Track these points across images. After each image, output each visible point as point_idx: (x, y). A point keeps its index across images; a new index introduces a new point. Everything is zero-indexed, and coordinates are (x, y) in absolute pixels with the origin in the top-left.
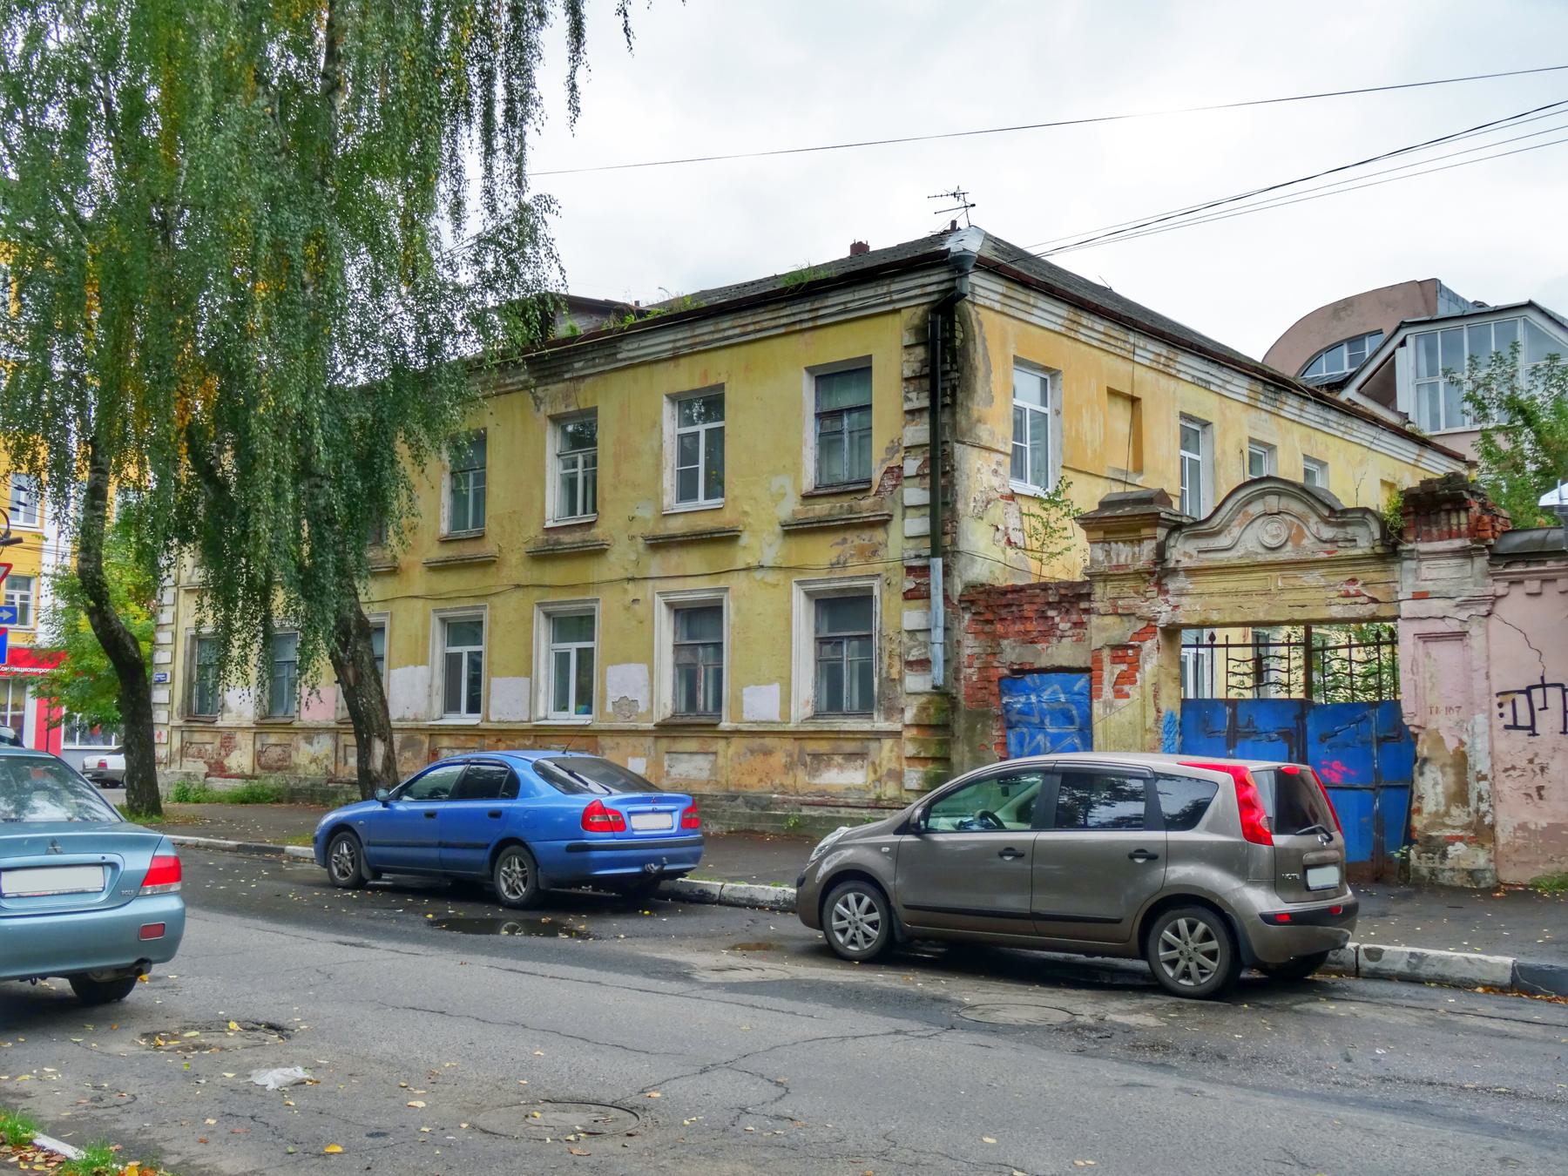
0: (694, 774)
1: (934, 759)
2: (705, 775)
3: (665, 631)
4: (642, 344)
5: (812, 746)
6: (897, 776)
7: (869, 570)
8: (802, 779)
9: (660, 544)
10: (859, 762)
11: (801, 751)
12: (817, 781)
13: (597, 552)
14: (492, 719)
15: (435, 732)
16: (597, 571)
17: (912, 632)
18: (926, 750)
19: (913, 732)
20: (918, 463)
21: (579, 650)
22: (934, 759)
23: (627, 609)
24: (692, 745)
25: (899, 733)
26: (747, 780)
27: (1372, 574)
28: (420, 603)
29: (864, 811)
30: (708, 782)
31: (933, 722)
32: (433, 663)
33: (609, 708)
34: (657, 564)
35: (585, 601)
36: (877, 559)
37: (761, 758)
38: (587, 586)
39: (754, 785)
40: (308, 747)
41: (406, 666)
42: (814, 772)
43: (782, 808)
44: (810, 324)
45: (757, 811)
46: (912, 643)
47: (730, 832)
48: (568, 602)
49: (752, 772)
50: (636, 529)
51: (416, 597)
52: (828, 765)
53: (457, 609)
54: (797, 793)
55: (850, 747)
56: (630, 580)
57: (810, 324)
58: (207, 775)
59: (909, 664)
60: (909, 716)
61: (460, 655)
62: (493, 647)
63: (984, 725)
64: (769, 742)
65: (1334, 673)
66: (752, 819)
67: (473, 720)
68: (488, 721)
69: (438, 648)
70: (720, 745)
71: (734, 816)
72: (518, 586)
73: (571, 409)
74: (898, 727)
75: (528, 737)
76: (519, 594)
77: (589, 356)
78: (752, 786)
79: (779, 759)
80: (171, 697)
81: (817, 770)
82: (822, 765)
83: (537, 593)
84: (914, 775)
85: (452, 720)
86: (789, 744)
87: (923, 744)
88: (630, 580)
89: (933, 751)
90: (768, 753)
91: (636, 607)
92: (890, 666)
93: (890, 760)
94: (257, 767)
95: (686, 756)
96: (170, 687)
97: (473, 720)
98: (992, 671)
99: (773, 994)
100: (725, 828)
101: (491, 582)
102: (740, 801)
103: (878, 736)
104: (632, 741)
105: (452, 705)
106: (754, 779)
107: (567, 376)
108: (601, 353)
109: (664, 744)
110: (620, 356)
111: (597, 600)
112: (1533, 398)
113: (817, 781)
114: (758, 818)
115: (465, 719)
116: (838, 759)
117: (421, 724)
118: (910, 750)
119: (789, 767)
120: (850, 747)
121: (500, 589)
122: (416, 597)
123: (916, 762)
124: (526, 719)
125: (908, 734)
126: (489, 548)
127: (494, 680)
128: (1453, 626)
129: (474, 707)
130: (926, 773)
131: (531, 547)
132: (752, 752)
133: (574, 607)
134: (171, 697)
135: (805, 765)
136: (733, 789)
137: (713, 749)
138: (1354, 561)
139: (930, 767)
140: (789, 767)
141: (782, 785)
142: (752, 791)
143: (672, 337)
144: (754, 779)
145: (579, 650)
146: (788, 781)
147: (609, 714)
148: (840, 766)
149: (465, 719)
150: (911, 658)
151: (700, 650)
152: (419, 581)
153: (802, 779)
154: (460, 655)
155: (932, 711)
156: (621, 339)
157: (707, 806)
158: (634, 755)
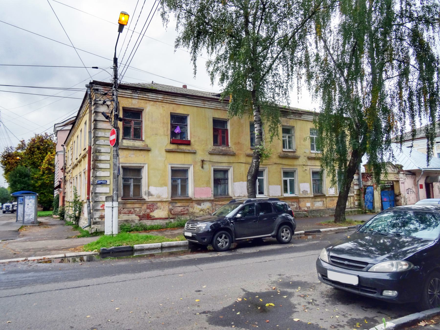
0: (319, 205)
1: (359, 200)
2: (321, 205)
3: (310, 177)
4: (196, 101)
6: (354, 203)
9: (310, 159)
13: (296, 158)
14: (270, 195)
16: (296, 162)
21: (290, 180)
22: (359, 200)
23: (304, 171)
24: (319, 200)
27: (396, 175)
33: (301, 192)
34: (309, 163)
38: (294, 165)
40: (199, 207)
41: (239, 181)
44: (165, 101)
48: (288, 168)
50: (305, 154)
51: (242, 163)
56: (304, 165)
57: (137, 98)
58: (140, 220)
59: (354, 184)
62: (297, 178)
64: (334, 198)
68: (269, 196)
72: (276, 164)
73: (288, 125)
74: (354, 195)
76: (276, 165)
77: (295, 115)
83: (281, 166)
85: (286, 195)
87: (357, 198)
88: (304, 165)
90: (333, 200)
94: (170, 214)
99: (310, 250)
102: (330, 210)
104: (308, 199)
105: (286, 191)
107: (288, 117)
108: (298, 115)
109: (313, 200)
110: (302, 117)
111: (297, 169)
112: (347, 154)
118: (356, 199)
121: (271, 164)
122: (242, 163)
128: (403, 182)
129: (292, 191)
131: (279, 154)
138: (395, 173)
143: (216, 104)
145: (290, 180)
149: (288, 195)
151: (317, 181)
156: (304, 114)
158: (308, 202)
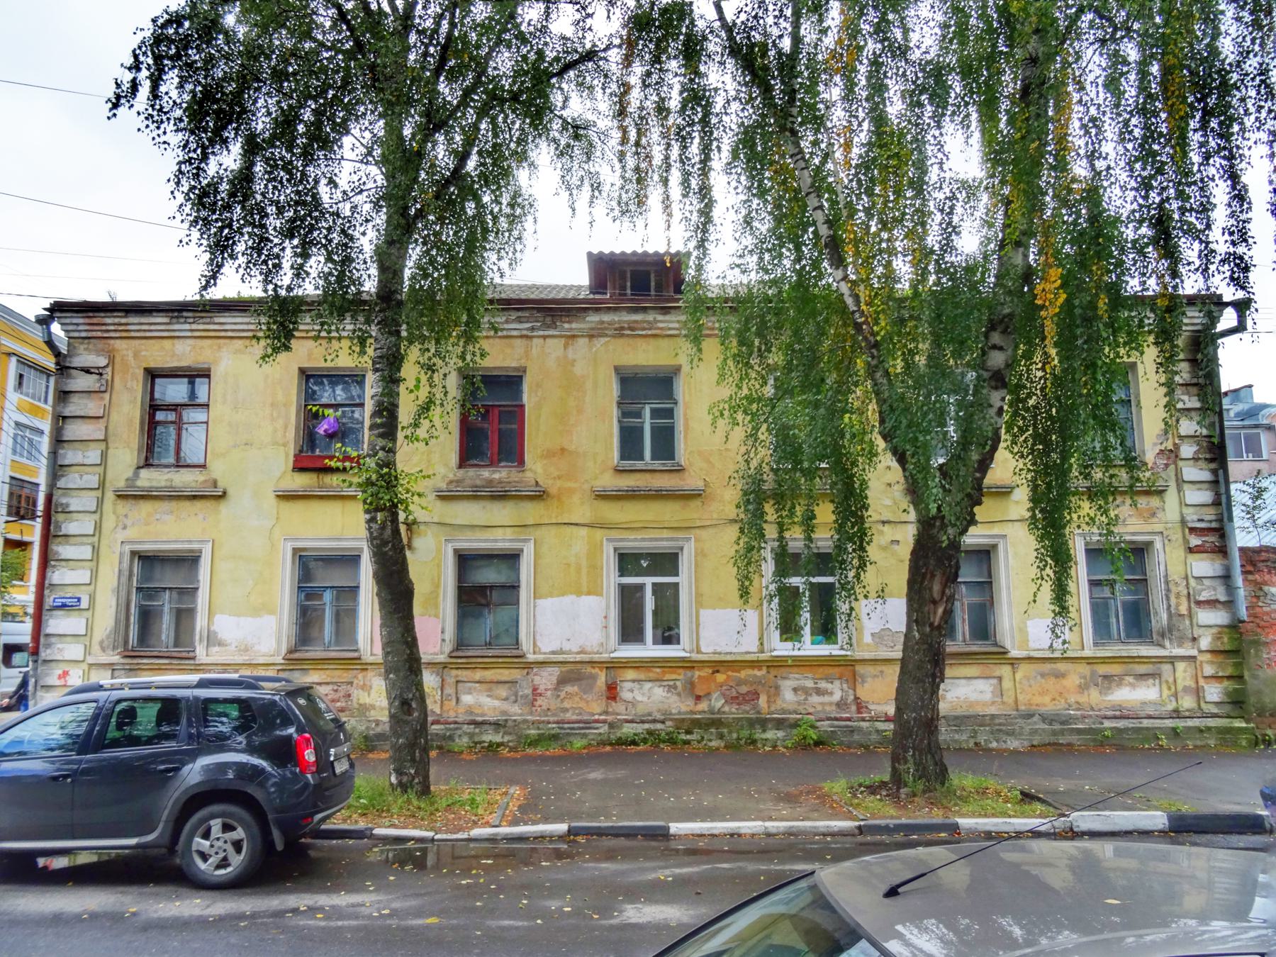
2: (988, 696)
5: (1103, 669)
6: (1198, 692)
7: (1149, 528)
8: (1093, 696)
10: (1151, 681)
11: (1093, 673)
12: (1110, 698)
14: (703, 650)
15: (613, 666)
17: (1199, 579)
18: (1223, 670)
19: (1208, 657)
20: (1195, 448)
21: (654, 585)
22: (1229, 678)
25: (1195, 657)
26: (1037, 699)
28: (583, 532)
29: (1166, 721)
30: (993, 703)
31: (1227, 647)
32: (608, 592)
35: (677, 539)
36: (1155, 520)
37: (1052, 680)
39: (1047, 704)
42: (1105, 690)
43: (1083, 723)
44: (189, 334)
45: (1057, 727)
46: (1199, 587)
47: (1033, 746)
49: (1042, 694)
52: (1120, 684)
53: (643, 540)
54: (1092, 709)
55: (1142, 669)
60: (1205, 643)
61: (641, 588)
63: (1257, 651)
64: (1061, 666)
65: (1190, 616)
66: (1054, 733)
67: (824, 650)
68: (699, 652)
69: (611, 579)
70: (1005, 671)
71: (1034, 732)
74: (1194, 652)
75: (760, 668)
78: (1044, 705)
79: (1073, 680)
80: (89, 627)
81: (1109, 688)
82: (1114, 684)
84: (1213, 690)
85: (783, 649)
86: (1084, 669)
89: (1229, 671)
91: (896, 547)
92: (1178, 605)
93: (1184, 679)
95: (963, 681)
96: (89, 614)
97: (824, 650)
98: (1258, 610)
100: (1026, 743)
101: (695, 516)
102: (1036, 718)
103: (1172, 660)
106: (1047, 699)
113: (1110, 698)
114: (1062, 732)
115: (649, 650)
116: (1131, 679)
117: (596, 657)
118: (1209, 670)
119: (1083, 688)
120: (1142, 669)
123: (1213, 680)
124: (755, 650)
125: (1201, 658)
126: (691, 481)
127: (705, 614)
129: (668, 635)
130: (1225, 688)
132: (1043, 675)
133: (665, 544)
134: (89, 627)
135: (1097, 685)
136: (1023, 708)
137: (997, 674)
139: (1226, 683)
140: (1083, 688)
141: (1078, 703)
142: (1043, 710)
144: (1047, 699)
145: (654, 585)
146: (1083, 699)
147: (868, 645)
148: (1131, 685)
150: (1201, 599)
152: (581, 510)
153: (1093, 696)
154: (641, 588)
155: (1226, 640)
157: (1000, 724)
